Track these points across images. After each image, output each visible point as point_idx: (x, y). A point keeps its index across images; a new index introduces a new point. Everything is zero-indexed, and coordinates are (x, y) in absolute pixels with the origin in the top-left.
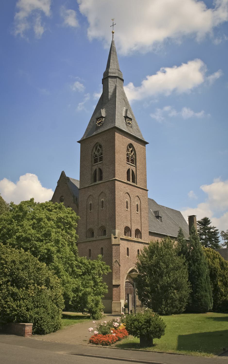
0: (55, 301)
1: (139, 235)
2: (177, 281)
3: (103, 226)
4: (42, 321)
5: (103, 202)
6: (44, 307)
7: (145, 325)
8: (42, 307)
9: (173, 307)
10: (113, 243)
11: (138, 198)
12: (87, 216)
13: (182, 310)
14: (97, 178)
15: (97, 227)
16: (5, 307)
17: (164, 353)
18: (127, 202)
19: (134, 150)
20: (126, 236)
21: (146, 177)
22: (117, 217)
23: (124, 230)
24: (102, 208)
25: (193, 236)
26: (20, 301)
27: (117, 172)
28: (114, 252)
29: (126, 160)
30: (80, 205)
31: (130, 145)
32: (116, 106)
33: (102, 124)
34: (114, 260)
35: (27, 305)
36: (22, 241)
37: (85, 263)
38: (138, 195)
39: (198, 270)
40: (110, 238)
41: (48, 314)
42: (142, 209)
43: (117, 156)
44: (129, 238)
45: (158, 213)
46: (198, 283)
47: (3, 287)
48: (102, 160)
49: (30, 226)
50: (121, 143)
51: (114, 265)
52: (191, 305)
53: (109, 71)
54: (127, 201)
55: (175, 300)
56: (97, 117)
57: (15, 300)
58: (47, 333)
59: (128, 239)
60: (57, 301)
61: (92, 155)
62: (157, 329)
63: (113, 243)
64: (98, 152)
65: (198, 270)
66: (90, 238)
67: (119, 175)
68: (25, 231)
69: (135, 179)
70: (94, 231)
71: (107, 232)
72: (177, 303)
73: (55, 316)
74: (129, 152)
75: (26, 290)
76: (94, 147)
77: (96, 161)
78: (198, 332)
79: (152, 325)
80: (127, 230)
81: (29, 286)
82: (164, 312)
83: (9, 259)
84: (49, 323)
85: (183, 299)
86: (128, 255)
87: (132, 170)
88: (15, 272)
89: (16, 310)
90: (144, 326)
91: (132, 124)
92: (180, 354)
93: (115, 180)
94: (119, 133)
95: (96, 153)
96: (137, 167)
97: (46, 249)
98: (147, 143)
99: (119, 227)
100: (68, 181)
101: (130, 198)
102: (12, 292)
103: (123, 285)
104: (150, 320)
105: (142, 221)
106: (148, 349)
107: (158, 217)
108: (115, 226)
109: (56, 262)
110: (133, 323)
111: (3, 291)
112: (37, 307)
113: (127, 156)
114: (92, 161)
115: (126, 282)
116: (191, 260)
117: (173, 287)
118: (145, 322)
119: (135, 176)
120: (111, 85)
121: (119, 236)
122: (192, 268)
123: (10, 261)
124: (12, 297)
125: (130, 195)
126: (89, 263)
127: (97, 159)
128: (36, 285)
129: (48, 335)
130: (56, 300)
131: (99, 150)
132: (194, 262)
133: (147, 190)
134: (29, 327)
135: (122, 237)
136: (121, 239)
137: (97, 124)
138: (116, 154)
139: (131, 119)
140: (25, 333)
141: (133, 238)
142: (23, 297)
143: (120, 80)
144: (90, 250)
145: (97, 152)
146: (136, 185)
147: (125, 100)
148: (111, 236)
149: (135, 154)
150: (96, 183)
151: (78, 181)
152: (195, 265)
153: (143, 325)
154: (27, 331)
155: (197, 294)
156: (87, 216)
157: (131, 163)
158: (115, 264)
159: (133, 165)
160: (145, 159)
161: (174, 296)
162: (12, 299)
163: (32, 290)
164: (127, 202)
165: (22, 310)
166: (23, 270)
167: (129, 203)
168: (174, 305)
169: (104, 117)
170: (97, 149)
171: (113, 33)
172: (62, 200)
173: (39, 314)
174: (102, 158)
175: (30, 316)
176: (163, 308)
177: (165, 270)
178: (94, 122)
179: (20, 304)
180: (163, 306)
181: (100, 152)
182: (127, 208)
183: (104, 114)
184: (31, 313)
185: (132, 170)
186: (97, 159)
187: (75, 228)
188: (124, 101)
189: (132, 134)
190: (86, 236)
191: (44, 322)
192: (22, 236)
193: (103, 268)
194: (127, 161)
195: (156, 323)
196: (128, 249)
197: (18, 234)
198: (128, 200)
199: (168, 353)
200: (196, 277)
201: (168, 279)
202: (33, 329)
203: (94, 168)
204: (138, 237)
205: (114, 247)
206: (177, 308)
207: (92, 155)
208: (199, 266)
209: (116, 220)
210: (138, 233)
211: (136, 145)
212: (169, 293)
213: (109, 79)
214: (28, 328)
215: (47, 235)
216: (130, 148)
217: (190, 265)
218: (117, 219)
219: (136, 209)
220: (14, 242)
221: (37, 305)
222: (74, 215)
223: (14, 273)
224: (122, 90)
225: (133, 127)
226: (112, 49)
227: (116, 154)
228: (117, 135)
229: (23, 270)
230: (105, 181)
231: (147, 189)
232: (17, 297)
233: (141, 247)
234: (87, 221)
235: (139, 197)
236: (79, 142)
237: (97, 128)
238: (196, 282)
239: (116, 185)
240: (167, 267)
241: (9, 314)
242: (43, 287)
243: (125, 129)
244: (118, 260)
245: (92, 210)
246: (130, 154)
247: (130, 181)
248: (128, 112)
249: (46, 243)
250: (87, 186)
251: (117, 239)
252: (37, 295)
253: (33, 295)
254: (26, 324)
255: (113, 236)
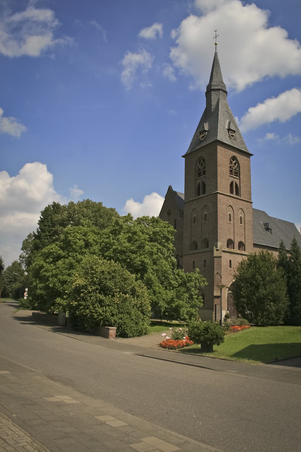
0: (140, 309)
1: (243, 248)
2: (273, 293)
3: (206, 239)
4: (125, 326)
5: (206, 215)
6: (127, 313)
7: (203, 332)
8: (126, 313)
9: (269, 319)
10: (215, 255)
11: (242, 211)
12: (191, 229)
13: (279, 322)
14: (201, 192)
15: (200, 240)
16: (93, 312)
17: (216, 358)
18: (230, 215)
19: (237, 162)
20: (229, 249)
21: (250, 190)
22: (219, 229)
23: (226, 242)
24: (206, 221)
25: (293, 249)
26: (106, 308)
27: (220, 185)
28: (215, 264)
29: (229, 172)
30: (184, 218)
31: (234, 158)
32: (219, 119)
33: (205, 137)
34: (216, 272)
35: (112, 311)
36: (118, 253)
37: (182, 275)
38: (242, 208)
39: (298, 282)
40: (212, 251)
41: (132, 320)
42: (246, 222)
43: (219, 169)
44: (232, 250)
45: (268, 225)
46: (297, 296)
47: (92, 294)
48: (205, 174)
49: (125, 239)
50: (223, 157)
51: (216, 277)
52: (289, 317)
53: (212, 83)
54: (230, 214)
55: (272, 312)
56: (200, 130)
57: (102, 306)
58: (130, 337)
59: (230, 251)
60: (143, 308)
61: (195, 169)
62: (214, 336)
63: (215, 255)
64: (202, 166)
65: (298, 282)
66: (194, 250)
67: (221, 188)
68: (120, 244)
69: (239, 192)
70: (198, 244)
71: (210, 245)
72: (273, 315)
73: (139, 322)
74: (232, 164)
75: (112, 297)
76: (197, 162)
77: (199, 175)
78: (279, 342)
79: (210, 332)
80: (230, 243)
81: (115, 294)
82: (260, 324)
83: (99, 270)
84: (132, 328)
85: (280, 311)
86: (230, 267)
87: (235, 182)
88: (103, 281)
89: (102, 315)
90: (202, 333)
91: (235, 137)
92: (230, 360)
93: (217, 193)
94: (221, 146)
95: (200, 167)
96: (241, 179)
97: (140, 261)
98: (252, 155)
99: (222, 240)
100: (175, 195)
101: (233, 210)
102: (99, 299)
103: (225, 296)
104: (208, 328)
105: (246, 234)
106: (208, 355)
107: (267, 229)
108: (217, 239)
109: (150, 274)
110: (193, 330)
111: (92, 298)
112: (122, 313)
113: (230, 168)
114: (195, 175)
115: (228, 294)
116: (291, 272)
117: (269, 299)
118: (203, 330)
119: (239, 189)
120: (214, 98)
121: (221, 248)
122: (292, 281)
123: (99, 272)
124: (100, 304)
125: (233, 207)
126: (186, 276)
127: (201, 173)
128: (121, 293)
129: (132, 338)
130: (142, 308)
131: (202, 164)
132: (294, 275)
133: (252, 203)
134: (113, 331)
135: (224, 250)
136: (223, 251)
137: (200, 138)
138: (218, 168)
139: (234, 131)
140: (109, 335)
141: (236, 250)
142: (108, 304)
143: (223, 92)
144: (194, 262)
145: (200, 166)
146: (240, 198)
147: (228, 112)
148: (213, 248)
149: (239, 166)
150: (199, 197)
151: (183, 194)
152: (294, 278)
153: (201, 332)
154: (111, 334)
155: (296, 307)
156: (191, 229)
157: (235, 175)
158: (216, 276)
159: (236, 177)
160: (249, 171)
161: (270, 308)
162: (99, 306)
163: (117, 297)
164: (230, 215)
165: (107, 315)
166: (110, 279)
167: (232, 215)
168: (270, 317)
169: (207, 131)
170: (201, 163)
171: (216, 44)
172: (170, 214)
173: (123, 319)
174: (205, 172)
175: (114, 320)
176: (259, 319)
177: (262, 283)
178: (197, 136)
179: (106, 310)
180: (258, 317)
181: (203, 166)
182: (230, 221)
183: (206, 128)
184: (115, 318)
185: (235, 182)
186: (201, 173)
187: (172, 242)
188: (227, 114)
189: (235, 146)
190: (191, 249)
191: (127, 326)
192: (117, 248)
193: (200, 281)
194: (230, 174)
195: (214, 331)
196: (230, 261)
197: (114, 247)
198: (231, 213)
199: (220, 359)
200: (296, 290)
201: (264, 291)
202: (117, 332)
203: (198, 182)
204: (241, 249)
205: (215, 259)
206: (274, 320)
207: (195, 169)
208: (299, 279)
209: (218, 232)
210: (241, 245)
211: (239, 157)
212: (265, 306)
213: (212, 92)
214: (112, 331)
215: (141, 247)
216: (234, 160)
217: (289, 277)
218: (219, 231)
219: (240, 221)
220: (112, 255)
221: (122, 311)
222: (171, 228)
223: (102, 283)
224: (225, 102)
225: (236, 139)
226: (215, 61)
227: (218, 167)
228: (219, 148)
229: (110, 279)
230: (207, 195)
231: (252, 201)
232: (104, 304)
233: (240, 259)
234: (191, 234)
235: (243, 209)
236: (183, 157)
237: (201, 142)
238: (295, 295)
239: (218, 198)
240: (264, 279)
241: (96, 319)
242: (127, 295)
243: (228, 142)
244: (219, 272)
245: (195, 224)
246: (233, 166)
247: (233, 194)
248: (231, 124)
249: (140, 255)
250: (192, 199)
251: (219, 252)
252: (122, 302)
253: (118, 303)
254: (110, 328)
255: (215, 249)
